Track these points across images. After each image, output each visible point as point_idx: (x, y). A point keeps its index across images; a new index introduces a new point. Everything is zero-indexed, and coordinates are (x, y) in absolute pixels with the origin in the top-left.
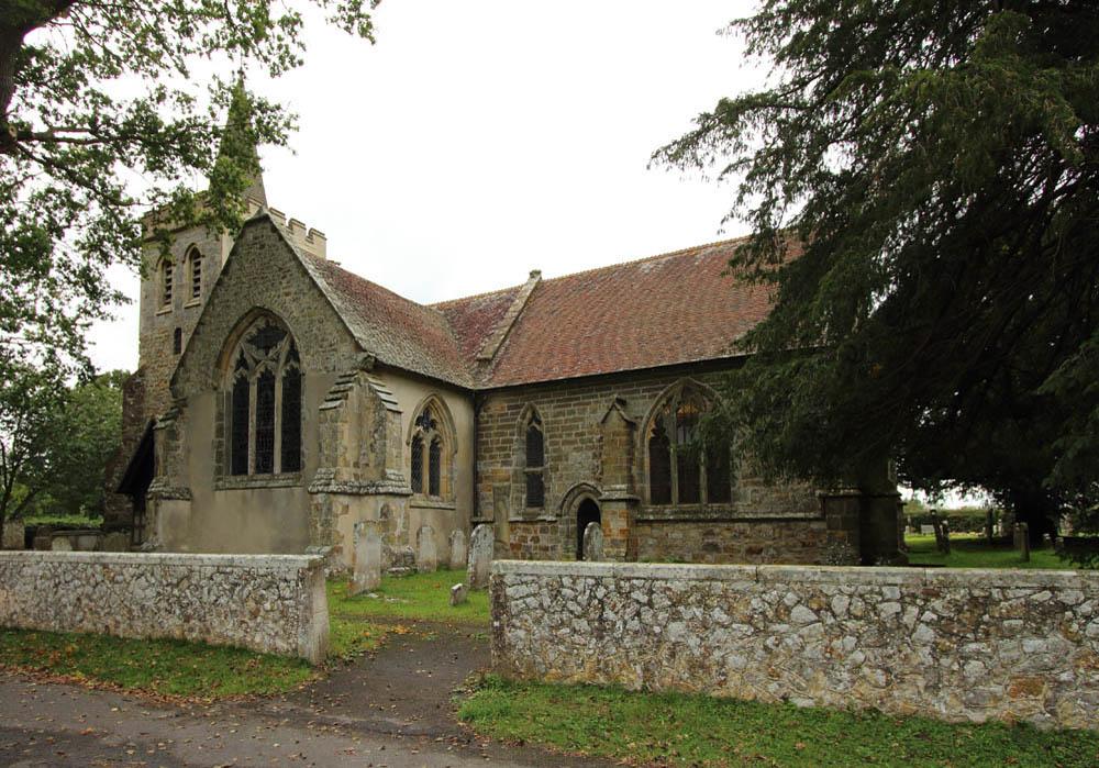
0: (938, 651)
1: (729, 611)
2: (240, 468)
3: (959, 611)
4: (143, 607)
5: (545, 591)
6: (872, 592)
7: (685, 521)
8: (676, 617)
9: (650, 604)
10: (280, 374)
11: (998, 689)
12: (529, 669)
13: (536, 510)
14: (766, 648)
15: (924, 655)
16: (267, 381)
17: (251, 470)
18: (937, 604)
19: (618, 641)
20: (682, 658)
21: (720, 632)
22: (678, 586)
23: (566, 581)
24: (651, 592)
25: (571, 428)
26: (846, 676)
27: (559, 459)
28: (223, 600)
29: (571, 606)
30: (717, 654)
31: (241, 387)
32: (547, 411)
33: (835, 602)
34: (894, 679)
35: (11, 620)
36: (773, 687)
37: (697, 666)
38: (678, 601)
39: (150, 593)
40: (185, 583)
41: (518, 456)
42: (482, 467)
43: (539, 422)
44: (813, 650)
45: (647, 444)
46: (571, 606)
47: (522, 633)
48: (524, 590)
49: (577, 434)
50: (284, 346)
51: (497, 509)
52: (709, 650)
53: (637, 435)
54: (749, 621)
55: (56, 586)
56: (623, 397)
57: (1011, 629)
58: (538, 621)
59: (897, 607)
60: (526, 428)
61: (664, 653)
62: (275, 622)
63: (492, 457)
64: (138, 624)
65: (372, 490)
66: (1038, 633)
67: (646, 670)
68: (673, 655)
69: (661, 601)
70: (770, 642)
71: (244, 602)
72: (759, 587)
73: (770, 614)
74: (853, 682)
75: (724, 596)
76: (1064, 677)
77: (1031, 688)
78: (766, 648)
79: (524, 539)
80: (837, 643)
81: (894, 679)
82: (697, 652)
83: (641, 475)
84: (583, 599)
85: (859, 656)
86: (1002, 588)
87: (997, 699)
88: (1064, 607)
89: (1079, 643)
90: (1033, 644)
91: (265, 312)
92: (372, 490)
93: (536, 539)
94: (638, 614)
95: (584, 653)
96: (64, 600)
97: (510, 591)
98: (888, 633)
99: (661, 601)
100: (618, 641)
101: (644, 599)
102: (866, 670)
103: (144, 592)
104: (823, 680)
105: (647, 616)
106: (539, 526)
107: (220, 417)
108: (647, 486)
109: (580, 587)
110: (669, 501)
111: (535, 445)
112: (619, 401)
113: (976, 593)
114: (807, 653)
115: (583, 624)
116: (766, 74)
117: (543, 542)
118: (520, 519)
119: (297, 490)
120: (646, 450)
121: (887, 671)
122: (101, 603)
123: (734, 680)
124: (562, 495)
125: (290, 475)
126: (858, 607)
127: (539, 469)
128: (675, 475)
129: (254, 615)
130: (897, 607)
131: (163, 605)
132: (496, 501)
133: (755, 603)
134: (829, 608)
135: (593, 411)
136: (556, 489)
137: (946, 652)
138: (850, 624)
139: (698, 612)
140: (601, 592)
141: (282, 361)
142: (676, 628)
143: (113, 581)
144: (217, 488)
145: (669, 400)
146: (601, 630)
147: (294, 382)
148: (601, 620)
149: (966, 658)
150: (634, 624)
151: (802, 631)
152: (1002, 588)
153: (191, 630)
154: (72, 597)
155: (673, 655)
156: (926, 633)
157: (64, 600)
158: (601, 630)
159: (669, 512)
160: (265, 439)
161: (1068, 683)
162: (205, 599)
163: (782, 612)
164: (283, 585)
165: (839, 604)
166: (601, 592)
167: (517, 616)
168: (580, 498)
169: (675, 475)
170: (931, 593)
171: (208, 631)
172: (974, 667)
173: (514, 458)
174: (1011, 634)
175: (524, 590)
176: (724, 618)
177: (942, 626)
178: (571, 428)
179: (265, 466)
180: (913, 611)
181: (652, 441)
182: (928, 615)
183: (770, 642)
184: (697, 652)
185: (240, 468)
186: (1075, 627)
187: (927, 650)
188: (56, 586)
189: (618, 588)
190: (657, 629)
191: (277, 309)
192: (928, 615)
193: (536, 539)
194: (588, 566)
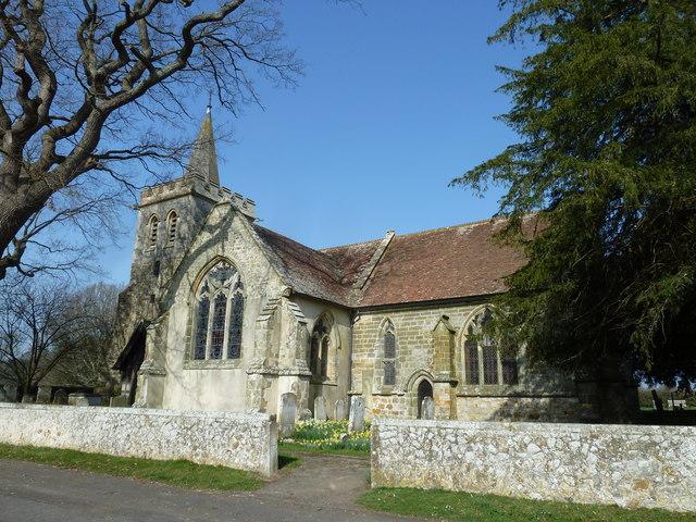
0: (599, 466)
1: (497, 446)
2: (200, 356)
3: (608, 446)
4: (168, 441)
5: (400, 435)
6: (566, 436)
7: (488, 396)
8: (469, 449)
9: (456, 442)
10: (230, 296)
11: (628, 487)
12: (392, 478)
13: (390, 386)
14: (515, 466)
15: (592, 470)
16: (221, 300)
17: (207, 357)
18: (597, 442)
19: (440, 463)
20: (473, 473)
21: (492, 457)
22: (471, 433)
23: (412, 429)
24: (456, 436)
25: (414, 333)
26: (556, 481)
27: (405, 353)
28: (217, 438)
29: (415, 443)
30: (491, 470)
31: (204, 304)
32: (398, 319)
33: (549, 442)
34: (579, 482)
35: (84, 448)
36: (520, 487)
37: (479, 476)
38: (471, 440)
39: (174, 433)
40: (195, 428)
41: (379, 351)
42: (354, 358)
43: (393, 329)
44: (539, 467)
45: (463, 345)
46: (415, 443)
47: (388, 458)
48: (389, 434)
49: (418, 338)
50: (234, 279)
51: (365, 386)
52: (486, 467)
53: (456, 339)
54: (507, 451)
55: (115, 427)
56: (447, 315)
57: (632, 455)
58: (397, 451)
59: (578, 444)
60: (384, 332)
61: (464, 469)
62: (248, 450)
63: (361, 351)
64: (165, 451)
65: (287, 372)
66: (644, 456)
67: (454, 478)
68: (468, 470)
69: (461, 440)
70: (518, 462)
71: (230, 439)
72: (511, 433)
73: (517, 447)
74: (559, 483)
75: (494, 439)
76: (658, 479)
77: (641, 485)
78: (515, 466)
79: (382, 406)
80: (550, 463)
81: (579, 482)
82: (481, 468)
83: (459, 365)
84: (421, 439)
85: (561, 470)
86: (627, 435)
87: (629, 492)
88: (655, 444)
89: (663, 462)
90: (643, 463)
91: (224, 260)
92: (287, 372)
93: (390, 407)
94: (450, 448)
95: (422, 469)
96: (119, 436)
97: (381, 435)
98: (575, 458)
99: (461, 440)
100: (440, 463)
101: (453, 439)
102: (566, 478)
103: (170, 432)
104: (545, 483)
105: (455, 448)
106: (392, 398)
107: (190, 322)
108: (463, 372)
109: (419, 433)
110: (477, 382)
111: (390, 345)
112: (444, 316)
113: (615, 436)
114: (536, 469)
115: (421, 453)
116: (516, 137)
117: (395, 409)
118: (380, 392)
119: (238, 371)
120: (463, 349)
121: (575, 477)
122: (143, 438)
123: (500, 483)
124: (407, 377)
125: (233, 361)
126: (560, 444)
127: (392, 360)
128: (481, 365)
129: (236, 446)
130: (578, 444)
131: (181, 439)
132: (364, 380)
133: (509, 441)
134: (546, 445)
135: (429, 320)
136: (403, 373)
137: (603, 467)
138: (557, 453)
139: (481, 446)
140: (430, 436)
141: (232, 287)
142: (470, 456)
143: (151, 425)
144: (184, 368)
145: (477, 317)
146: (431, 456)
147: (239, 303)
148: (431, 451)
149: (612, 470)
150: (448, 454)
151: (533, 457)
152: (627, 435)
153: (197, 455)
154: (125, 435)
155: (468, 470)
156: (593, 458)
157: (119, 436)
158: (431, 456)
159: (477, 390)
160: (218, 338)
161: (660, 483)
162: (207, 436)
163: (523, 447)
164: (253, 430)
165: (551, 443)
166: (430, 436)
167: (385, 449)
168: (420, 379)
169: (481, 365)
170: (594, 437)
171: (207, 456)
172: (616, 475)
173: (376, 352)
174: (631, 457)
175: (389, 434)
176: (494, 450)
177: (601, 454)
178: (414, 333)
179: (217, 353)
180: (586, 446)
181: (467, 343)
182: (593, 449)
183: (518, 462)
184: (481, 468)
185: (200, 356)
186: (661, 454)
187: (594, 466)
188: (115, 427)
189: (439, 434)
190: (460, 456)
191: (232, 257)
192: (593, 449)
193: (390, 407)
194: (425, 423)
